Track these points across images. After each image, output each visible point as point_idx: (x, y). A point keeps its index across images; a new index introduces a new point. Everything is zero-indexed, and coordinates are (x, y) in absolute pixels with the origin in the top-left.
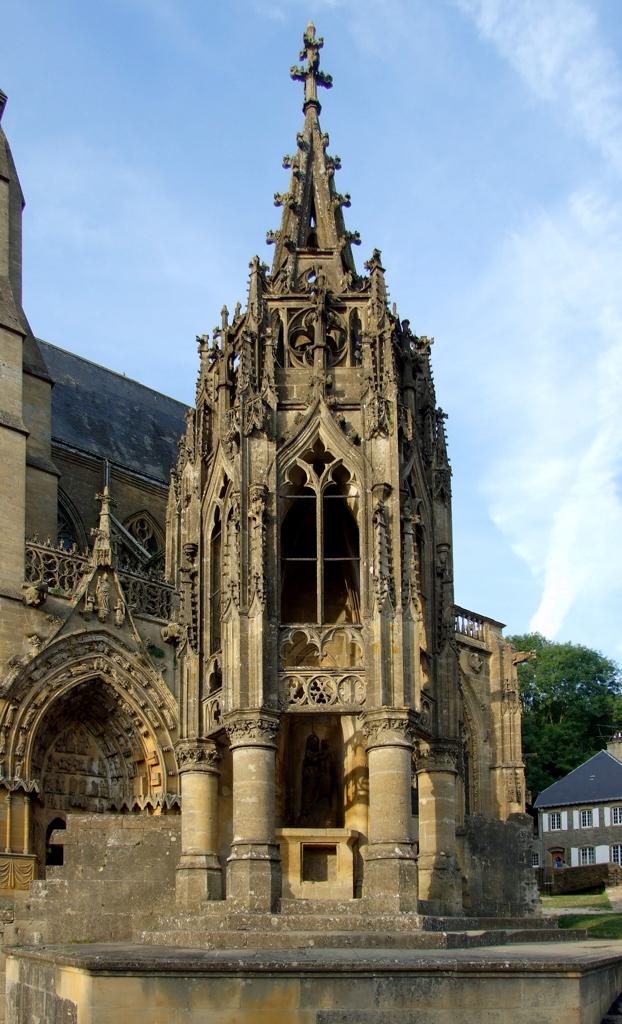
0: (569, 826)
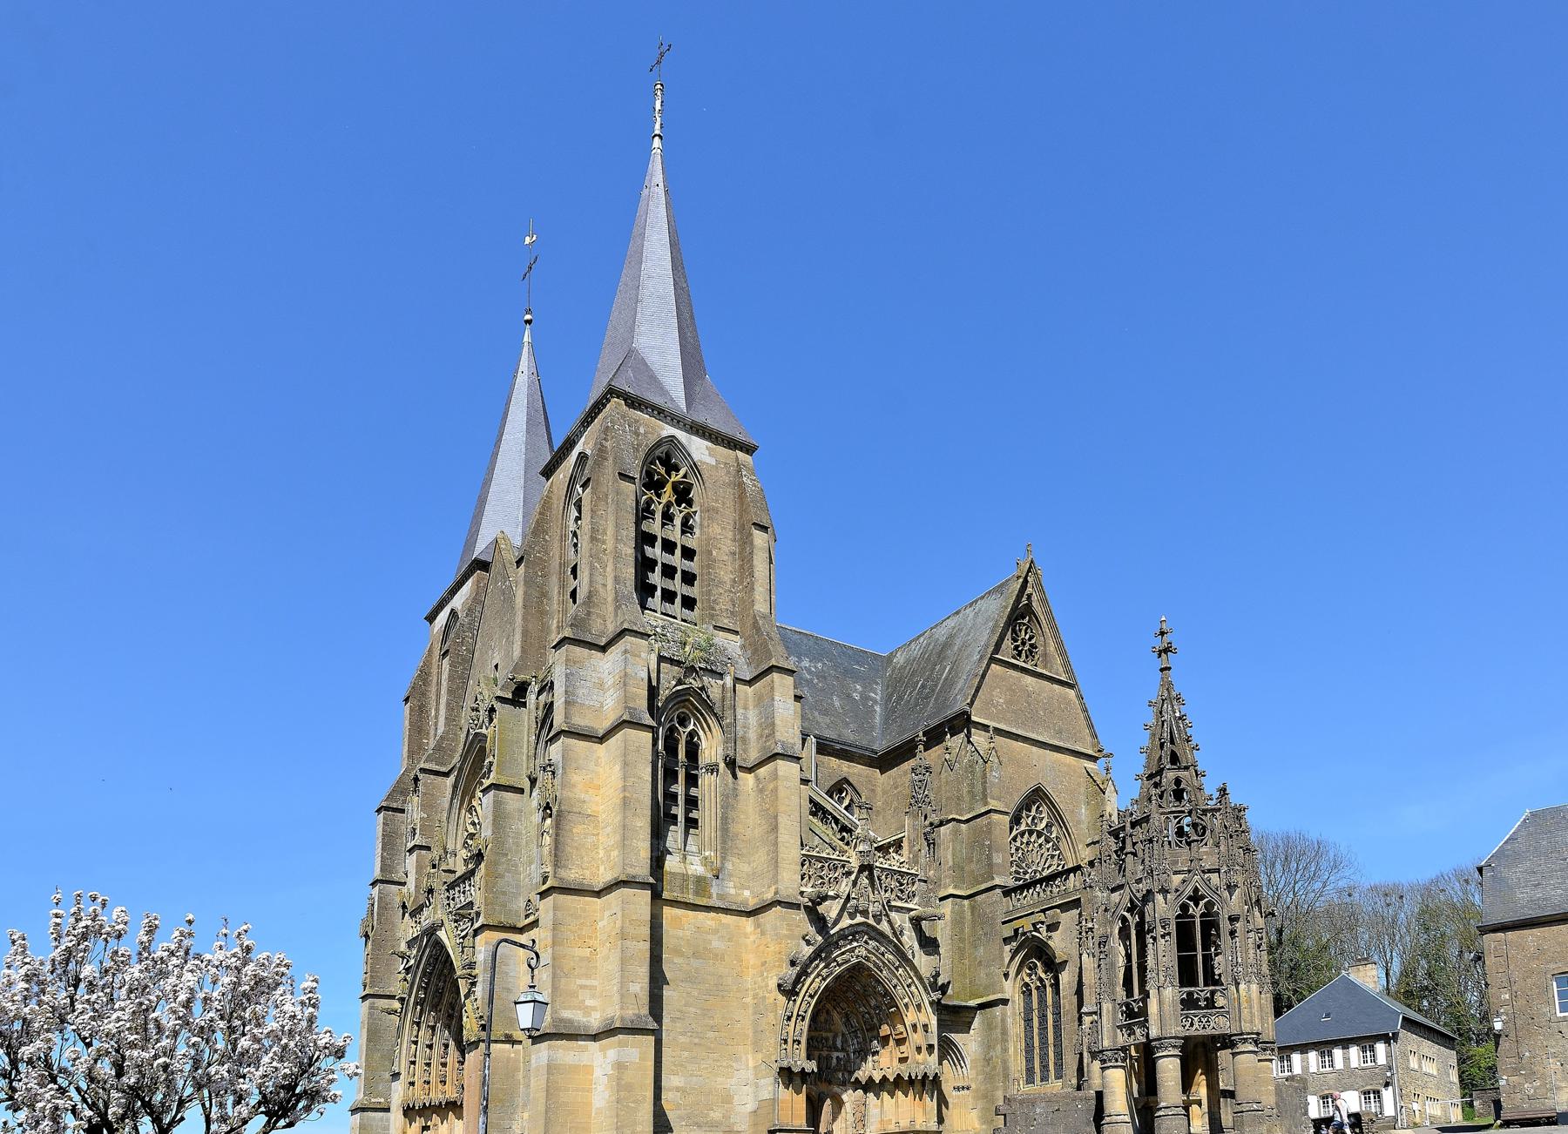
0: (974, 722)
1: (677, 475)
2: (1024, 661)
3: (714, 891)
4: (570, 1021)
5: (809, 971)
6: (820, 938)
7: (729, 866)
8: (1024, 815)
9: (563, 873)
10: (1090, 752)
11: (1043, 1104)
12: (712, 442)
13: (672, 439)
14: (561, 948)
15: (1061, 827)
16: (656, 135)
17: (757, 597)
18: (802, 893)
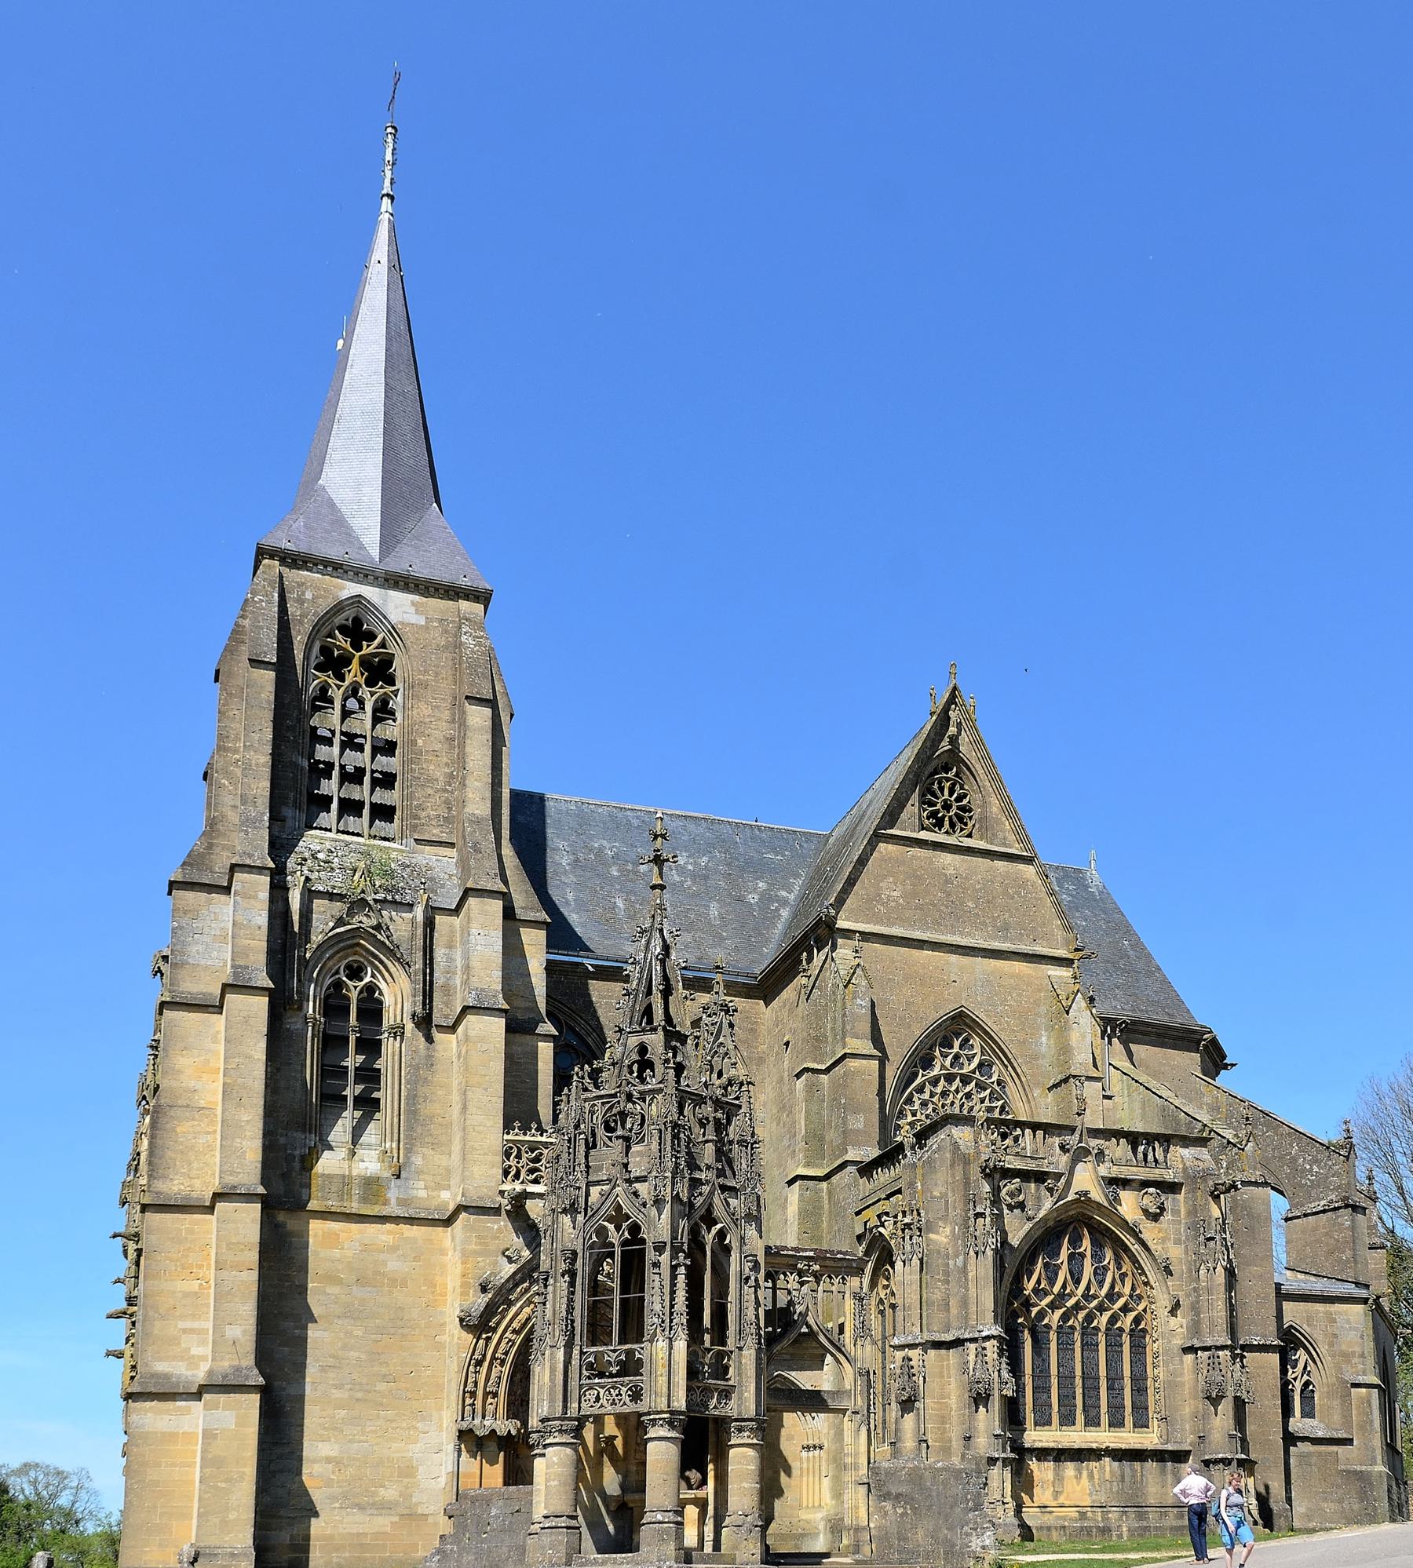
1: (368, 646)
2: (947, 833)
3: (393, 1194)
4: (167, 1376)
5: (512, 1297)
6: (528, 1252)
7: (417, 1160)
8: (937, 1053)
9: (160, 1186)
10: (1061, 953)
11: (500, 1503)
12: (422, 595)
13: (358, 599)
14: (156, 1282)
15: (1006, 1067)
16: (383, 195)
17: (470, 795)
18: (502, 1193)
